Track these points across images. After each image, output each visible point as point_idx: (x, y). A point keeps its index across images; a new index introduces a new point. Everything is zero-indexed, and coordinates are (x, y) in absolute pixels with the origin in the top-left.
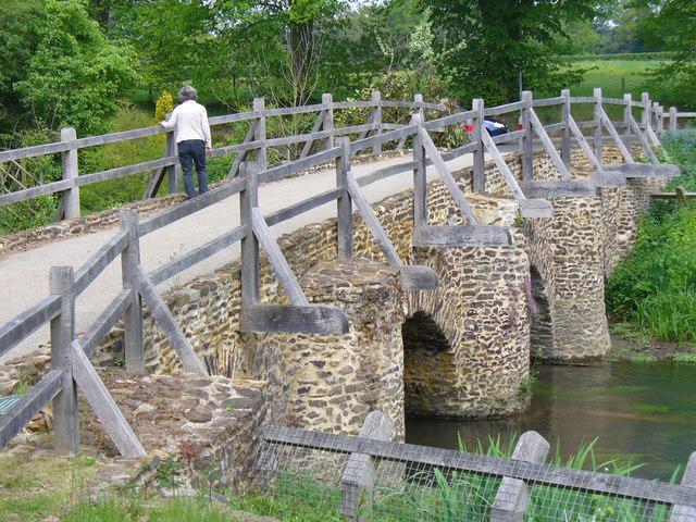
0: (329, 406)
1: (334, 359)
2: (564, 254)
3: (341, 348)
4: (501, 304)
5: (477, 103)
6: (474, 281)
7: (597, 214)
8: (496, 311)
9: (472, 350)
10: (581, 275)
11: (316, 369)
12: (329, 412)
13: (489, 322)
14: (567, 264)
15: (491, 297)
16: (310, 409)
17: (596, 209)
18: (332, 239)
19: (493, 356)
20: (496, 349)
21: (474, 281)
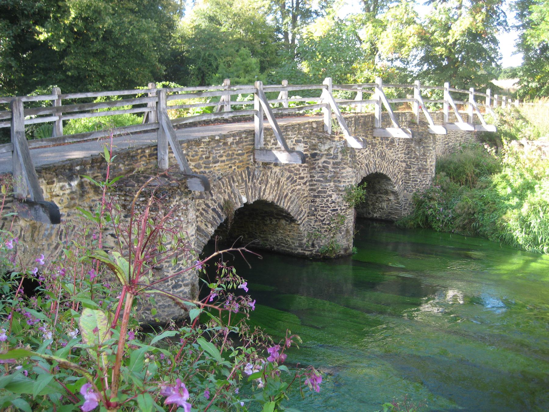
2: (410, 168)
4: (331, 197)
5: (446, 85)
6: (315, 183)
8: (327, 201)
9: (313, 222)
10: (419, 180)
11: (113, 239)
13: (323, 207)
14: (411, 174)
15: (325, 192)
18: (150, 155)
19: (325, 227)
20: (328, 222)
21: (315, 183)
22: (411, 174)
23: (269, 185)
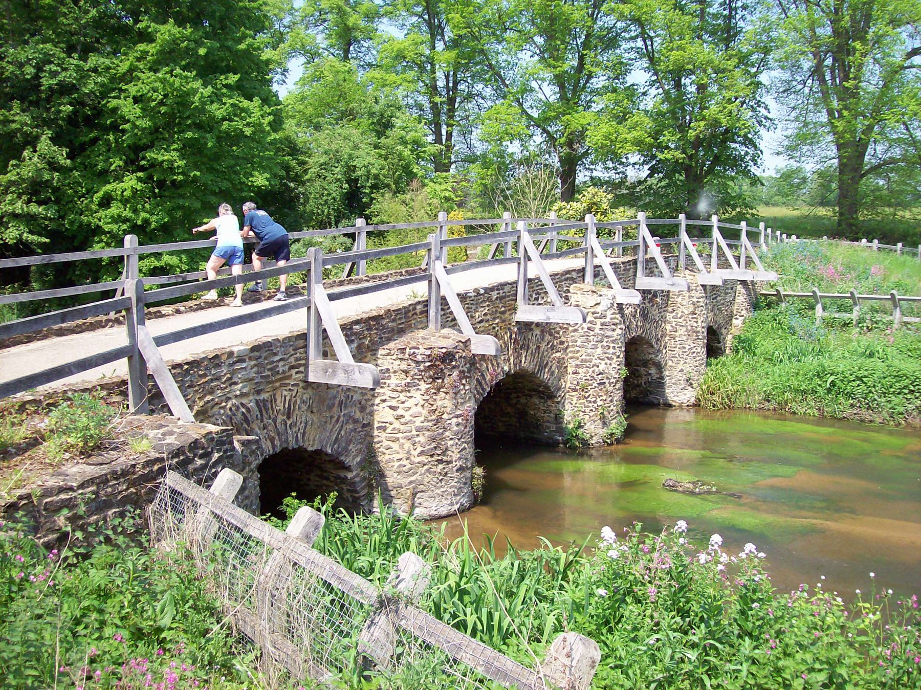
0: (402, 441)
1: (406, 405)
3: (411, 397)
6: (578, 349)
7: (702, 304)
12: (402, 446)
16: (386, 443)
17: (701, 300)
18: (421, 313)
19: (590, 405)
21: (578, 349)
22: (677, 339)
23: (530, 351)
